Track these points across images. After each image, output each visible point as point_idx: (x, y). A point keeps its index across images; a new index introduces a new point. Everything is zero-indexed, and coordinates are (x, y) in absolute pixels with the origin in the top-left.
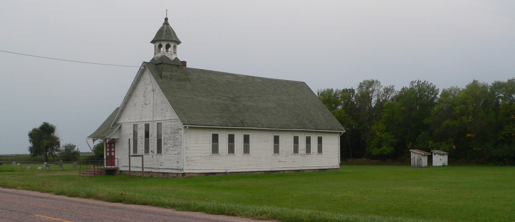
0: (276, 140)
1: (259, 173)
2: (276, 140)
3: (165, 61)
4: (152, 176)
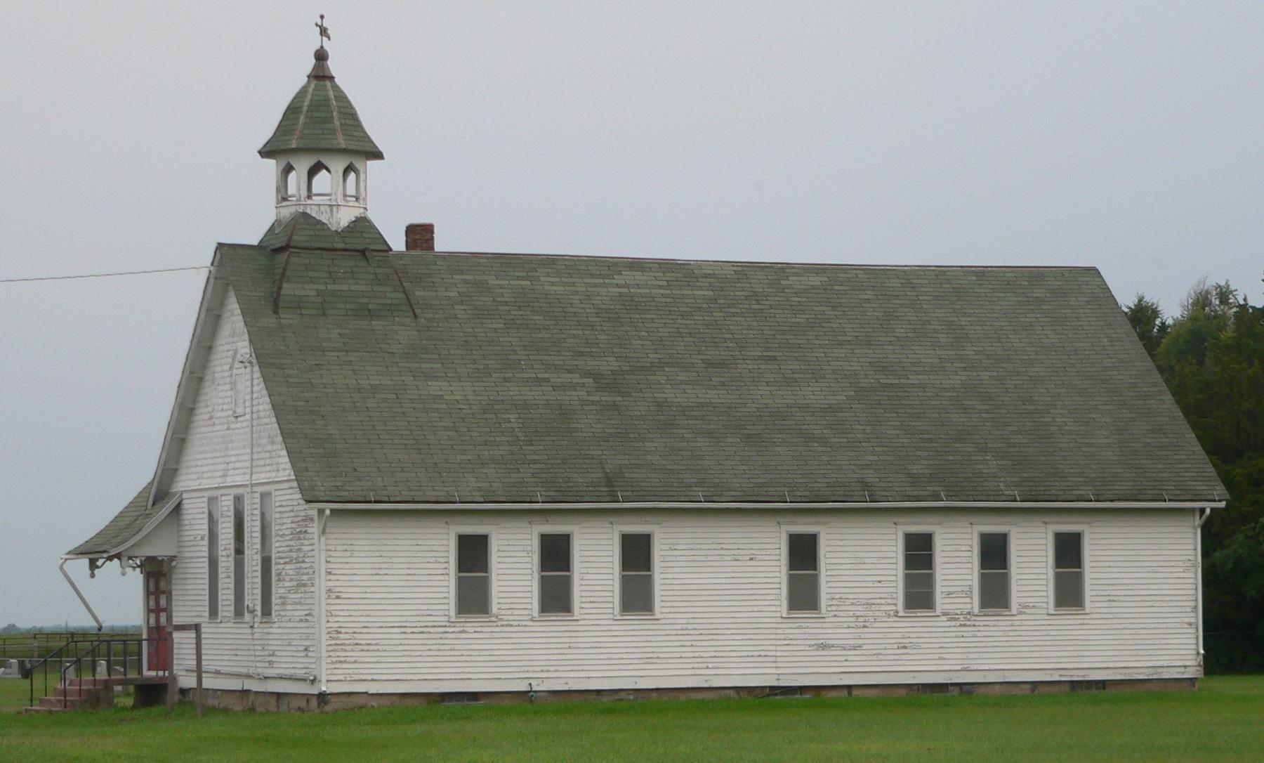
0: (803, 553)
1: (712, 695)
2: (803, 553)
3: (298, 239)
4: (252, 710)
